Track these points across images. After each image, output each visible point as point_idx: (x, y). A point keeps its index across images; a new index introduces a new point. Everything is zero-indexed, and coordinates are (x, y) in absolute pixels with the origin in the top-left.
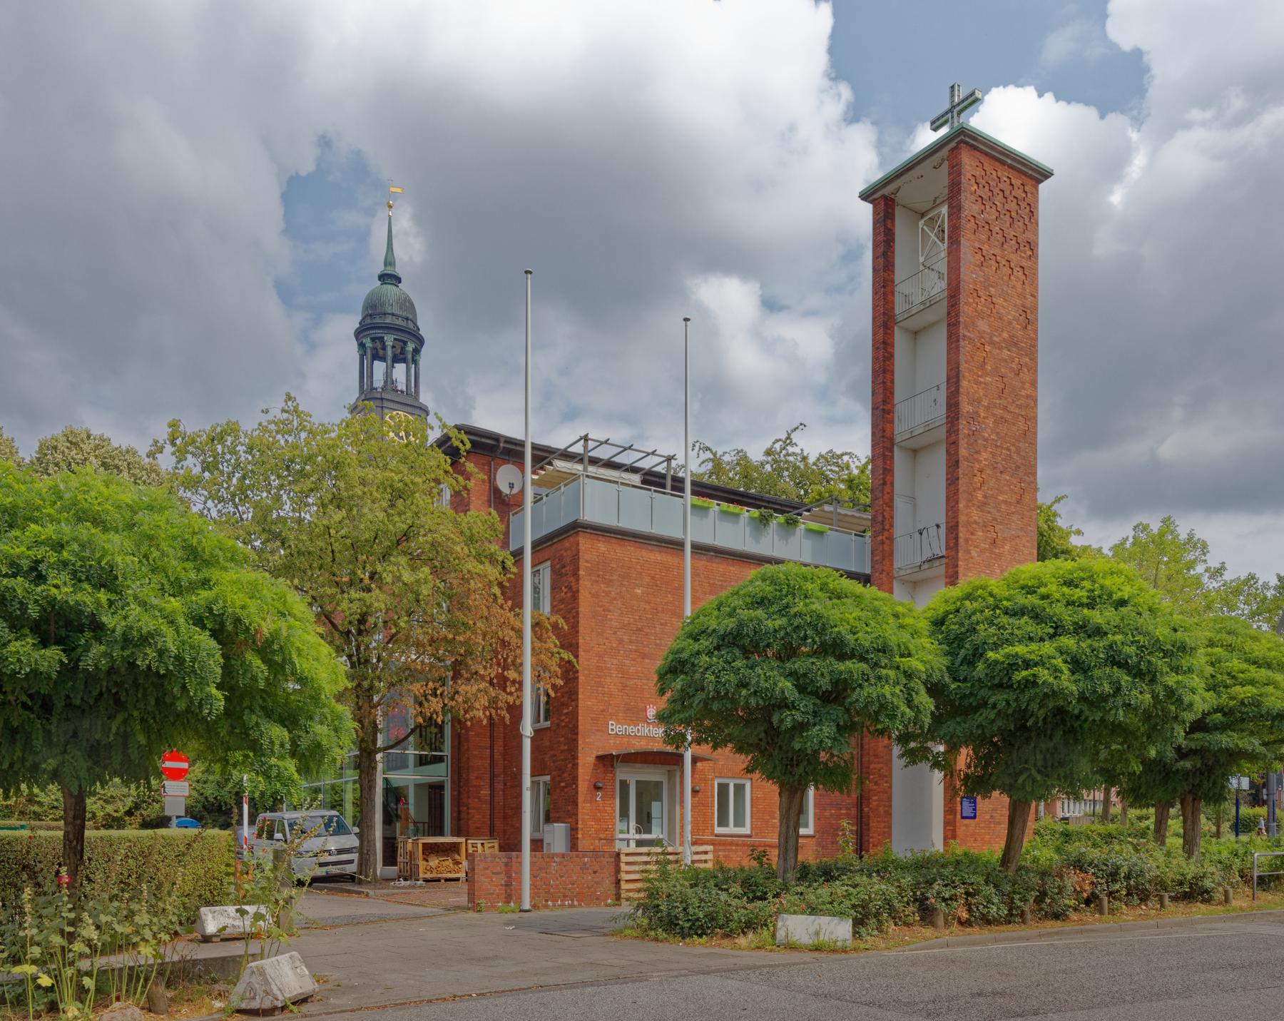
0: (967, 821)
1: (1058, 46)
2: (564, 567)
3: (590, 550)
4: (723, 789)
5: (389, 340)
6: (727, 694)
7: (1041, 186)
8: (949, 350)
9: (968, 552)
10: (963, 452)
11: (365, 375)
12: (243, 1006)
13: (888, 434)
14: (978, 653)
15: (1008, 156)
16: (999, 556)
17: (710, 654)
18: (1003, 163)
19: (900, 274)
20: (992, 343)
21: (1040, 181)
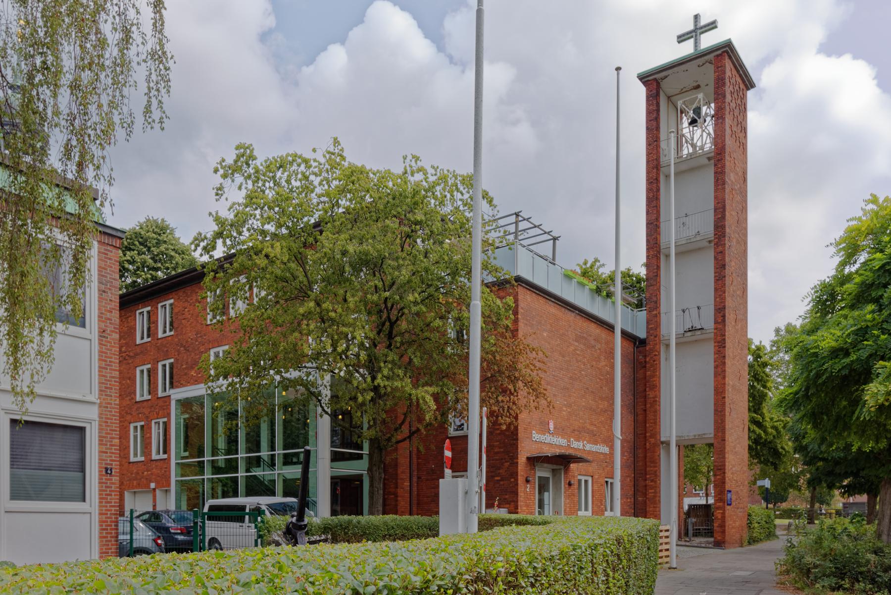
4: (580, 481)
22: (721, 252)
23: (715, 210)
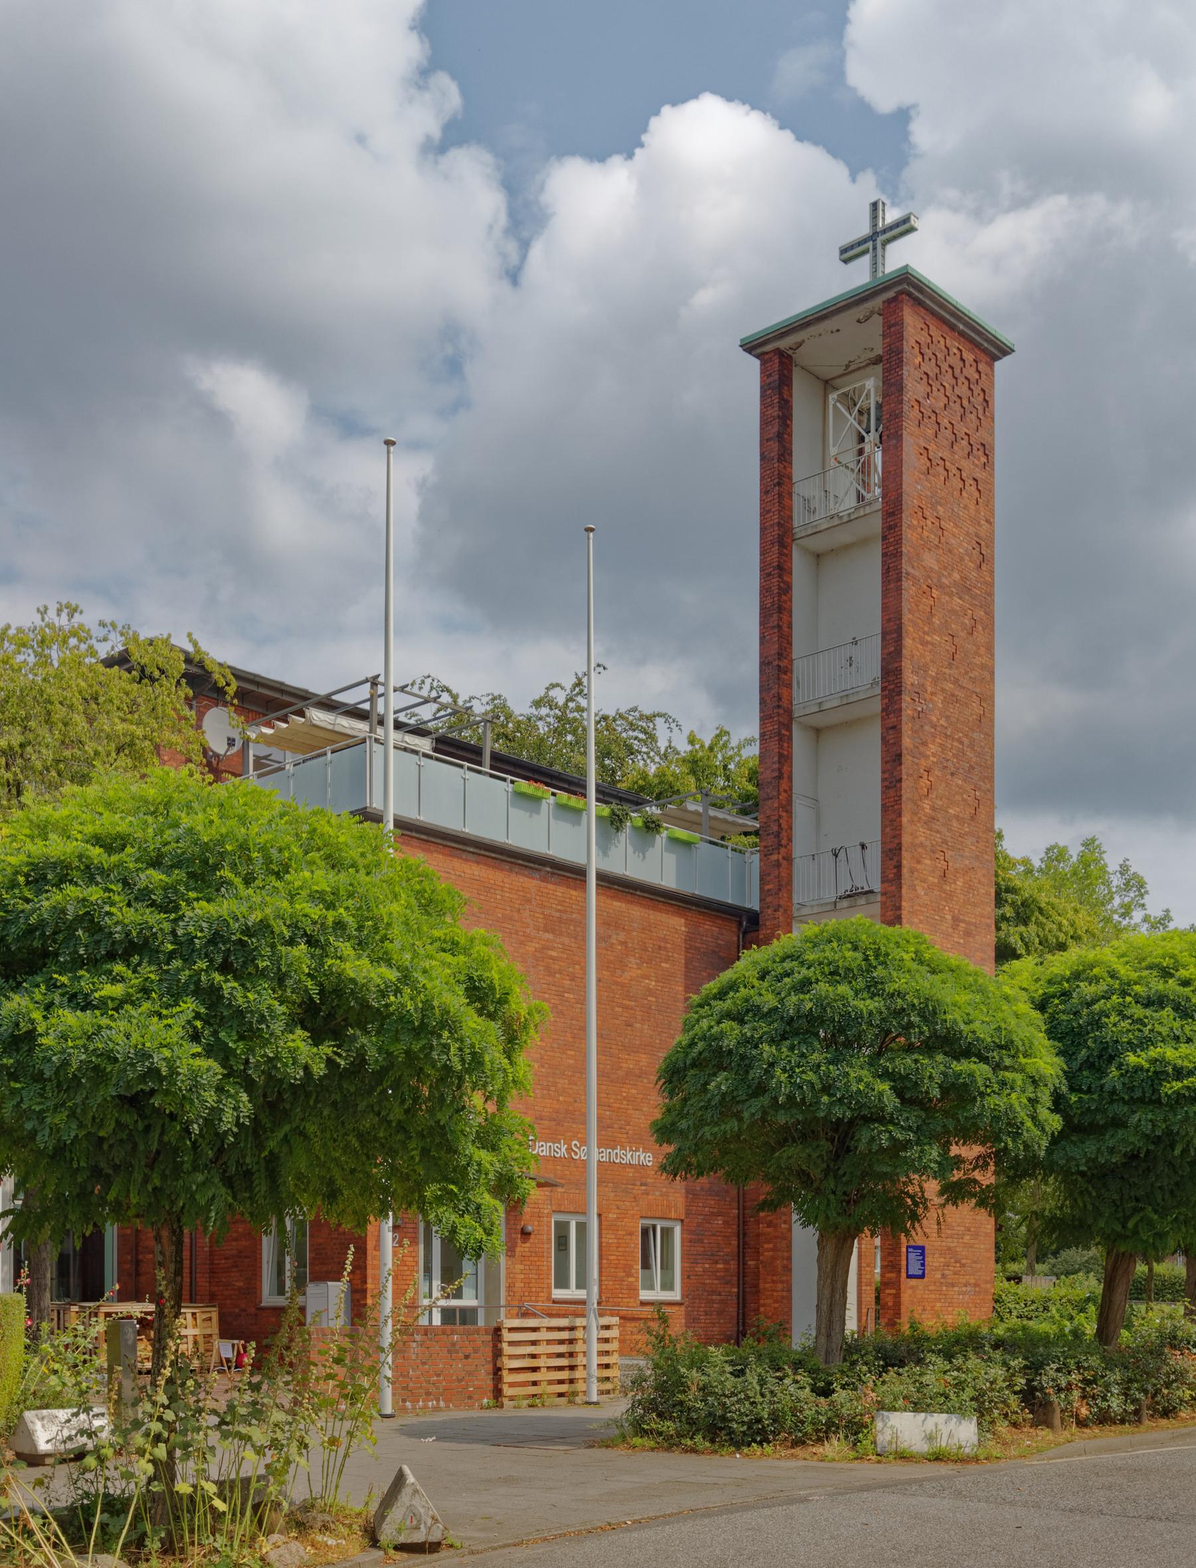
0: (914, 1282)
1: (795, 70)
4: (562, 1228)
6: (803, 1099)
7: (997, 364)
8: (885, 593)
10: (907, 742)
12: (402, 1539)
13: (785, 703)
14: (1108, 1054)
15: (959, 318)
16: (950, 896)
17: (772, 1041)
18: (953, 328)
19: (801, 466)
20: (941, 586)
21: (996, 358)
22: (894, 727)
23: (884, 634)
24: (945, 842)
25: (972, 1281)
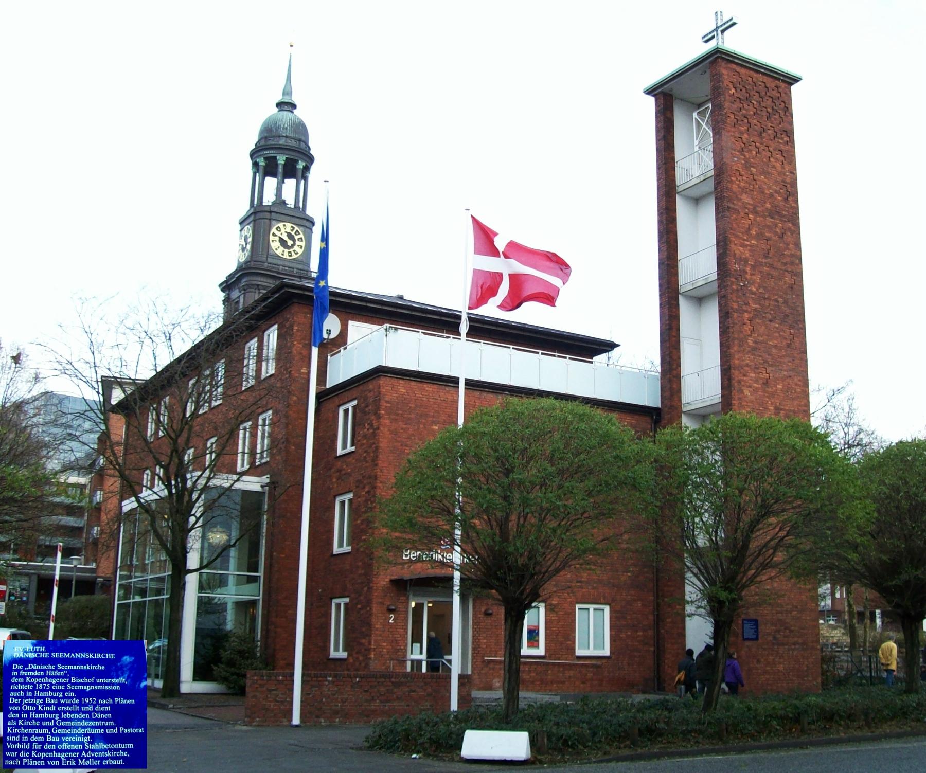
0: (748, 643)
2: (367, 406)
3: (390, 389)
5: (281, 160)
7: (793, 87)
9: (742, 392)
11: (257, 192)
21: (792, 84)
24: (766, 362)
25: (800, 641)
